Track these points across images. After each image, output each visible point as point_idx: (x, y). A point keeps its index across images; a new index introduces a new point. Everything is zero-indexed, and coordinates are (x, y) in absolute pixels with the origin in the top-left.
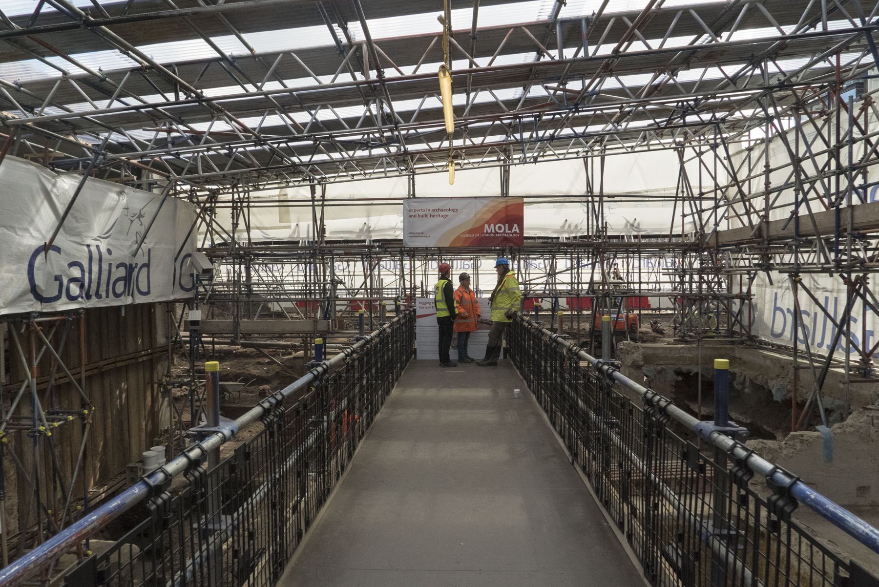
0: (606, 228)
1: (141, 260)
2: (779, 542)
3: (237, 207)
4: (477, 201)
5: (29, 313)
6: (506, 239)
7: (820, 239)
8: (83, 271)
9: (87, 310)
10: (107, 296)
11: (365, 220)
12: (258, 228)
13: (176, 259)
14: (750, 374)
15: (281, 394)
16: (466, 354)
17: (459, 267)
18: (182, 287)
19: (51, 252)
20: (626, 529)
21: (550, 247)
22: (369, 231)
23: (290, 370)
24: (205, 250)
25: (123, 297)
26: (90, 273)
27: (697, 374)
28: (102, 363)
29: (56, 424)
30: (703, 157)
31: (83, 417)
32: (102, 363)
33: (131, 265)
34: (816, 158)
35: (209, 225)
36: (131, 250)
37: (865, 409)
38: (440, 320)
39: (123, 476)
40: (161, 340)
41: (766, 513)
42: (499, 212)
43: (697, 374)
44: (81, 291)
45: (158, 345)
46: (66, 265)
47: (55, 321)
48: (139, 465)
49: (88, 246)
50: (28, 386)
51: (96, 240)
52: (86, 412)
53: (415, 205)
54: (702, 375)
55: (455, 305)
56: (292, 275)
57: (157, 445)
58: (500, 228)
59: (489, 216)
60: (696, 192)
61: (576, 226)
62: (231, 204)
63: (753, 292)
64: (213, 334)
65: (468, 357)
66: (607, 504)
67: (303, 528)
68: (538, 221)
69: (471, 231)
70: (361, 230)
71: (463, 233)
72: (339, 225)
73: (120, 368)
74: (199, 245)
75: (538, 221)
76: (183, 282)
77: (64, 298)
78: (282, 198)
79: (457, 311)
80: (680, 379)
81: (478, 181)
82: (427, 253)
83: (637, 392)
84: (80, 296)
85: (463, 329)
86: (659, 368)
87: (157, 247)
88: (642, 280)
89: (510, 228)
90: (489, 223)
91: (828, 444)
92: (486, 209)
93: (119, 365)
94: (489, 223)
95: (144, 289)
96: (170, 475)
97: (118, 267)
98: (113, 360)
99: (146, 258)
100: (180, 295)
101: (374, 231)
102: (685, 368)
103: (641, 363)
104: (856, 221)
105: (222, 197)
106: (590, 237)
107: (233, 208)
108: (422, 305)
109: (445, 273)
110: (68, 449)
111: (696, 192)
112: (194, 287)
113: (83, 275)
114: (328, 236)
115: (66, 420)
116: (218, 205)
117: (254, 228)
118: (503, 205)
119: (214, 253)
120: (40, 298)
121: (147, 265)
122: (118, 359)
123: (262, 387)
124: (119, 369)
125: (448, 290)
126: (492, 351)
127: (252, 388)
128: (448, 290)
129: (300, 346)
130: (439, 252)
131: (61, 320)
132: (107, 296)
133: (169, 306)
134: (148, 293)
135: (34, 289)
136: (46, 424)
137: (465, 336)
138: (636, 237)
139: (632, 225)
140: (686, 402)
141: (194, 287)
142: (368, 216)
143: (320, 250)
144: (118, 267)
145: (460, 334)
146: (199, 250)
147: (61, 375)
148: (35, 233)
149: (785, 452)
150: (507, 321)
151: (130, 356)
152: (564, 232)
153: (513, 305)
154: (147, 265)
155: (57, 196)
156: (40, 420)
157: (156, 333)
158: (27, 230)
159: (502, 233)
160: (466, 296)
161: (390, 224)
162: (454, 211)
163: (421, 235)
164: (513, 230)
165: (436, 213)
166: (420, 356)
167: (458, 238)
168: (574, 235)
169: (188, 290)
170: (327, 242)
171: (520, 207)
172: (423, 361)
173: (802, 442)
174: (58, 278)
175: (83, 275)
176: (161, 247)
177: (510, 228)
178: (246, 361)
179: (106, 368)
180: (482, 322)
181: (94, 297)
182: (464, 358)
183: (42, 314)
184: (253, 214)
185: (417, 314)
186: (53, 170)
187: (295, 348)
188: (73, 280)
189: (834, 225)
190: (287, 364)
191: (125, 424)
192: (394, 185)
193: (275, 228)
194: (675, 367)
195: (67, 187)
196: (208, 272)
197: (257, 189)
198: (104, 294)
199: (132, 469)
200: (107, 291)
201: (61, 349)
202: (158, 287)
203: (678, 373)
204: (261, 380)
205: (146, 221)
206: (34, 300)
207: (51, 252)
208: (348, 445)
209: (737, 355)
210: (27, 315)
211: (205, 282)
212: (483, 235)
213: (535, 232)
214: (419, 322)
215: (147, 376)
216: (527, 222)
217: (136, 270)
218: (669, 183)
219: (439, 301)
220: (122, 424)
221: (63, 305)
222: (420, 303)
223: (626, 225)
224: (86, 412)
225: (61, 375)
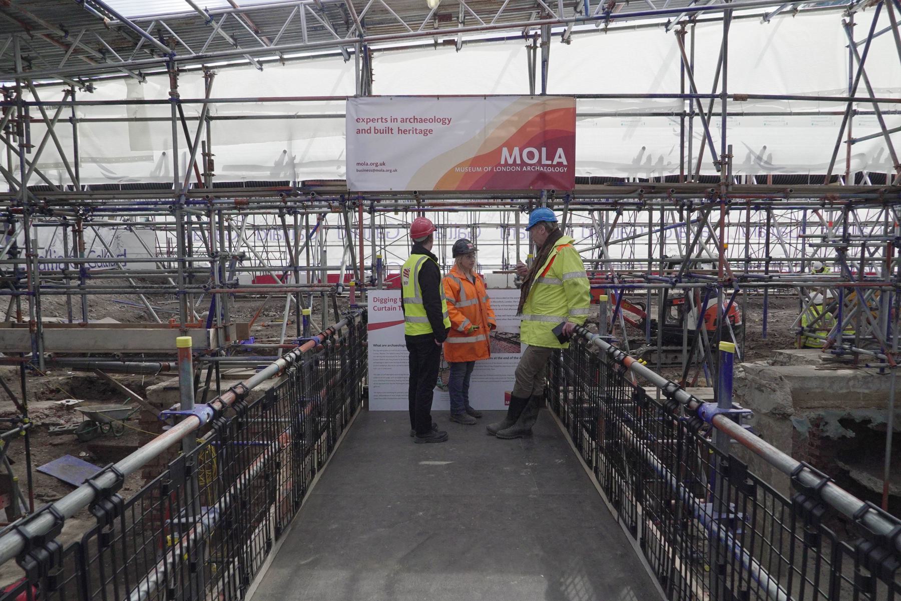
0: (730, 157)
2: (755, 506)
11: (283, 145)
12: (94, 160)
15: (221, 402)
16: (467, 402)
17: (452, 223)
20: (639, 535)
21: (613, 193)
22: (292, 165)
27: (885, 425)
38: (412, 342)
41: (852, 568)
42: (529, 124)
43: (885, 425)
53: (367, 109)
55: (445, 309)
58: (531, 155)
61: (661, 159)
65: (470, 411)
66: (618, 505)
67: (273, 536)
68: (601, 148)
69: (477, 161)
70: (278, 164)
72: (240, 155)
75: (601, 148)
79: (448, 324)
80: (851, 434)
82: (397, 200)
83: (781, 468)
85: (458, 357)
86: (813, 415)
88: (772, 255)
89: (550, 157)
92: (505, 118)
96: (122, 476)
101: (301, 164)
102: (858, 415)
106: (686, 177)
108: (378, 304)
109: (421, 239)
114: (220, 174)
117: (87, 160)
118: (538, 111)
125: (429, 275)
126: (521, 406)
128: (429, 275)
130: (418, 200)
137: (463, 371)
139: (759, 158)
140: (841, 464)
142: (290, 139)
143: (205, 197)
145: (454, 366)
150: (557, 345)
152: (640, 169)
153: (569, 312)
159: (535, 167)
160: (467, 288)
161: (323, 154)
166: (375, 404)
167: (451, 173)
168: (657, 175)
170: (216, 185)
171: (571, 116)
177: (550, 157)
180: (498, 338)
182: (461, 409)
184: (84, 135)
185: (370, 321)
192: (335, 76)
194: (843, 414)
203: (846, 422)
208: (328, 437)
213: (588, 169)
214: (373, 337)
222: (375, 300)
223: (748, 158)
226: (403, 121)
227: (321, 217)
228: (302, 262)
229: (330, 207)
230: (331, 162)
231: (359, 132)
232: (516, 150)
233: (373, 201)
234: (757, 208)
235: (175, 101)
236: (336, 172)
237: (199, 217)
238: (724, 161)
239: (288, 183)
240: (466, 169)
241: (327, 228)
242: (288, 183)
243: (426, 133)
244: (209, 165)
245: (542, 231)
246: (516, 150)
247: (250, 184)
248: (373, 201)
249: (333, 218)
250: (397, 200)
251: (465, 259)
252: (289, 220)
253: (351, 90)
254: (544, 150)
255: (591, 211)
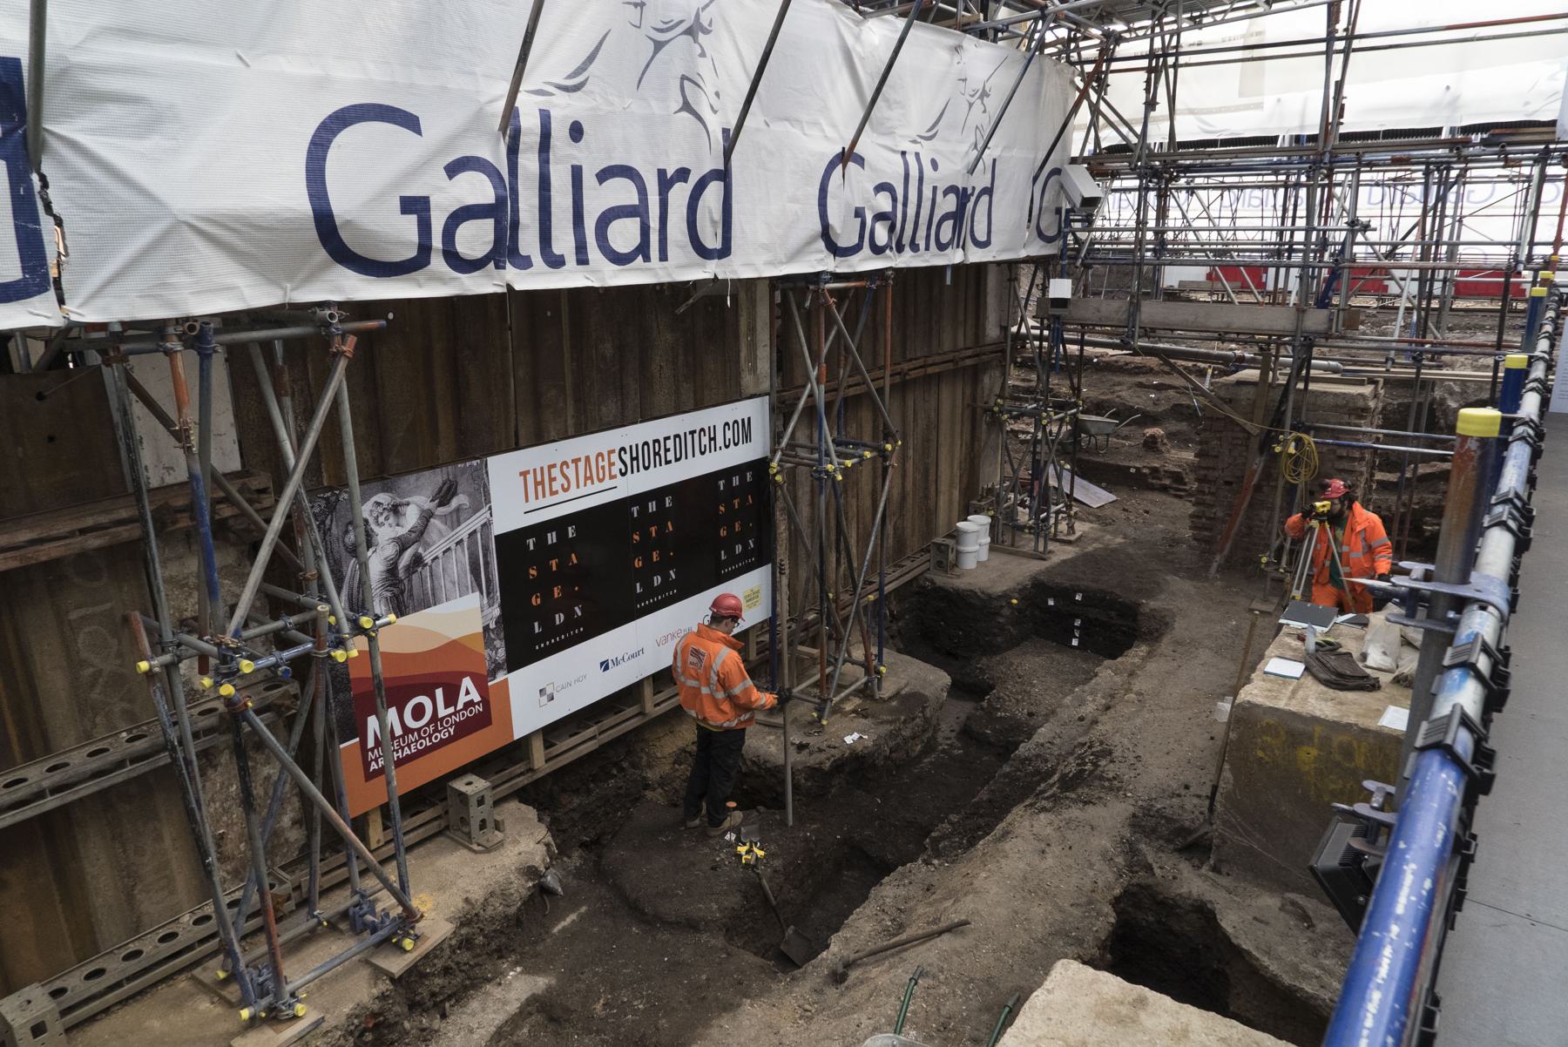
1: (980, 181)
3: (1159, 65)
5: (818, 274)
8: (894, 200)
9: (897, 271)
10: (927, 248)
12: (1191, 112)
13: (1035, 179)
18: (1040, 234)
19: (851, 165)
23: (1226, 407)
24: (1084, 160)
25: (949, 250)
26: (905, 205)
28: (906, 366)
29: (849, 463)
31: (884, 455)
32: (906, 366)
33: (965, 189)
34: (1324, 57)
35: (1095, 111)
36: (966, 162)
39: (927, 556)
40: (992, 332)
44: (890, 238)
45: (988, 340)
46: (871, 189)
47: (846, 290)
48: (950, 542)
49: (903, 153)
50: (811, 395)
51: (914, 142)
52: (889, 447)
56: (1247, 213)
57: (976, 513)
62: (1144, 63)
64: (1083, 326)
73: (930, 376)
74: (1075, 153)
76: (1042, 226)
77: (438, 263)
84: (888, 246)
87: (1006, 154)
93: (930, 370)
95: (982, 237)
97: (946, 193)
98: (920, 362)
99: (989, 175)
100: (1038, 249)
105: (1123, 49)
107: (1149, 70)
110: (854, 502)
112: (1061, 234)
113: (894, 207)
115: (861, 456)
116: (1114, 66)
119: (1101, 164)
120: (835, 250)
121: (988, 191)
122: (930, 361)
123: (1150, 431)
124: (928, 379)
127: (1125, 431)
129: (1253, 360)
131: (856, 288)
132: (927, 248)
133: (1011, 266)
134: (987, 244)
135: (826, 233)
136: (836, 460)
141: (1061, 234)
144: (946, 193)
146: (1074, 161)
147: (857, 379)
148: (829, 131)
151: (946, 357)
154: (988, 191)
155: (862, 59)
156: (827, 455)
157: (985, 318)
158: (816, 124)
169: (1049, 240)
174: (859, 213)
175: (894, 207)
176: (1015, 158)
178: (1116, 379)
179: (913, 374)
181: (907, 249)
183: (837, 277)
186: (856, 9)
187: (1241, 363)
188: (880, 217)
190: (1222, 393)
191: (932, 471)
193: (1228, 109)
195: (877, 42)
196: (1091, 203)
197: (1197, 23)
198: (922, 243)
199: (939, 546)
200: (928, 236)
201: (857, 337)
202: (1005, 234)
204: (1149, 419)
205: (994, 104)
206: (826, 252)
207: (851, 165)
210: (815, 278)
211: (1077, 225)
215: (968, 391)
217: (973, 199)
220: (926, 471)
221: (865, 262)
224: (889, 447)
225: (857, 379)
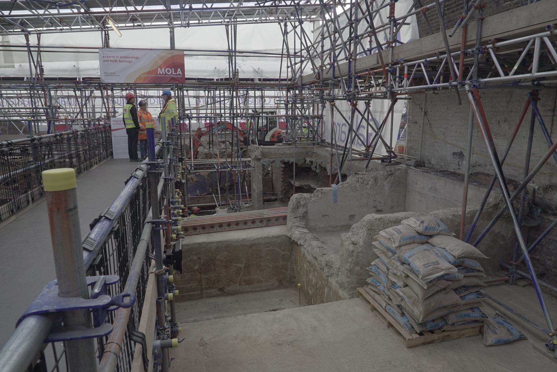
0: (238, 73)
4: (152, 51)
6: (173, 79)
7: (342, 79)
14: (319, 161)
22: (78, 70)
27: (293, 162)
30: (296, 29)
37: (356, 174)
43: (293, 162)
53: (106, 52)
54: (296, 163)
58: (168, 71)
59: (160, 63)
60: (292, 52)
63: (324, 114)
69: (149, 73)
71: (144, 74)
72: (53, 66)
75: (194, 67)
78: (6, 44)
81: (152, 38)
82: (122, 86)
86: (271, 160)
89: (176, 71)
90: (161, 67)
91: (335, 194)
94: (161, 67)
102: (286, 160)
103: (260, 157)
104: (356, 68)
108: (115, 123)
111: (292, 52)
114: (47, 74)
118: (170, 56)
138: (260, 80)
143: (40, 83)
149: (313, 199)
159: (170, 73)
161: (90, 66)
162: (136, 58)
163: (113, 74)
164: (178, 73)
165: (123, 59)
166: (115, 156)
167: (140, 77)
170: (46, 79)
171: (182, 57)
172: (117, 160)
173: (322, 193)
177: (176, 71)
189: (347, 71)
192: (92, 38)
203: (284, 163)
209: (315, 151)
212: (157, 76)
216: (186, 67)
218: (277, 46)
219: (127, 119)
226: (121, 57)
227: (92, 92)
228: (85, 110)
229: (95, 88)
230: (94, 69)
231: (104, 61)
232: (163, 69)
233: (113, 86)
234: (258, 90)
235: (28, 46)
236: (96, 74)
237: (38, 92)
238: (236, 73)
239: (76, 78)
240: (146, 75)
241: (95, 97)
242: (76, 78)
243: (130, 62)
244: (42, 70)
245: (166, 97)
246: (163, 69)
247: (61, 79)
248: (113, 86)
249: (97, 93)
250: (122, 86)
251: (143, 107)
252: (78, 93)
253: (99, 44)
254: (173, 69)
255: (205, 91)
